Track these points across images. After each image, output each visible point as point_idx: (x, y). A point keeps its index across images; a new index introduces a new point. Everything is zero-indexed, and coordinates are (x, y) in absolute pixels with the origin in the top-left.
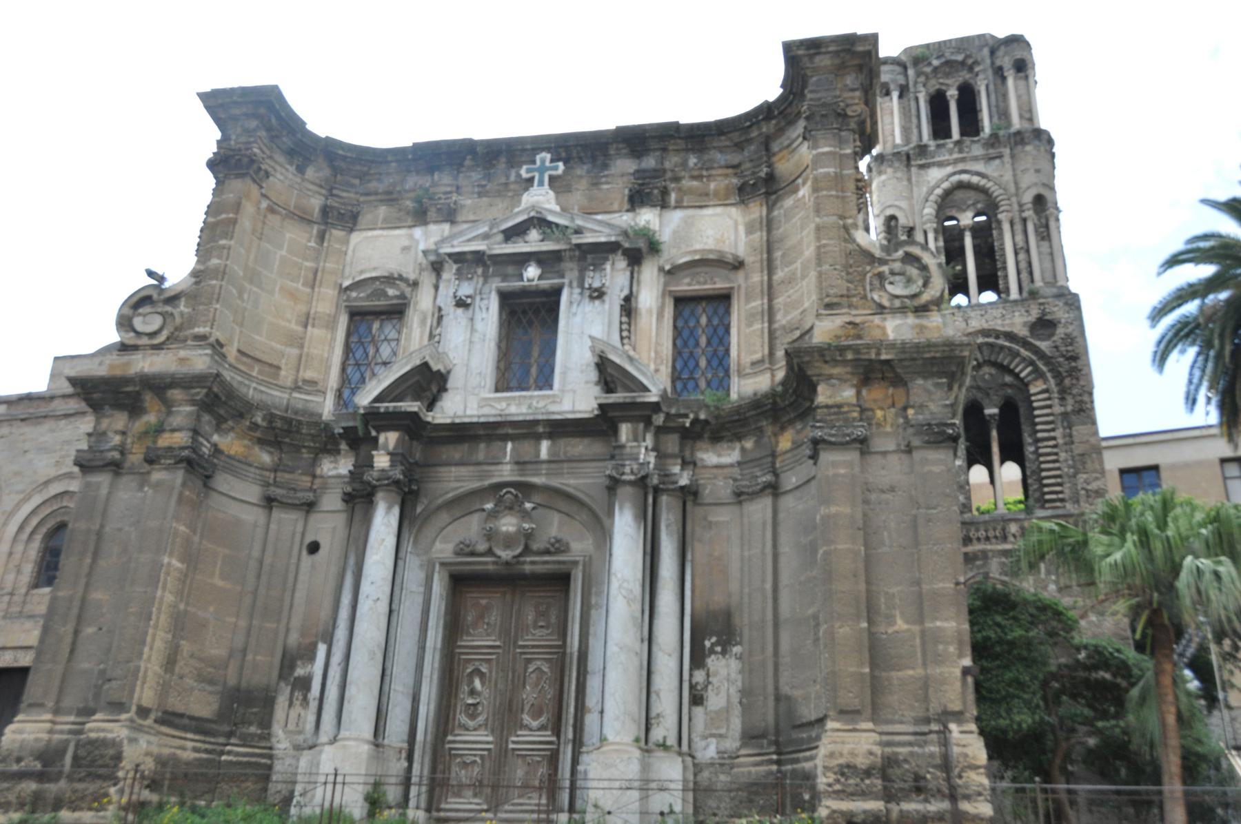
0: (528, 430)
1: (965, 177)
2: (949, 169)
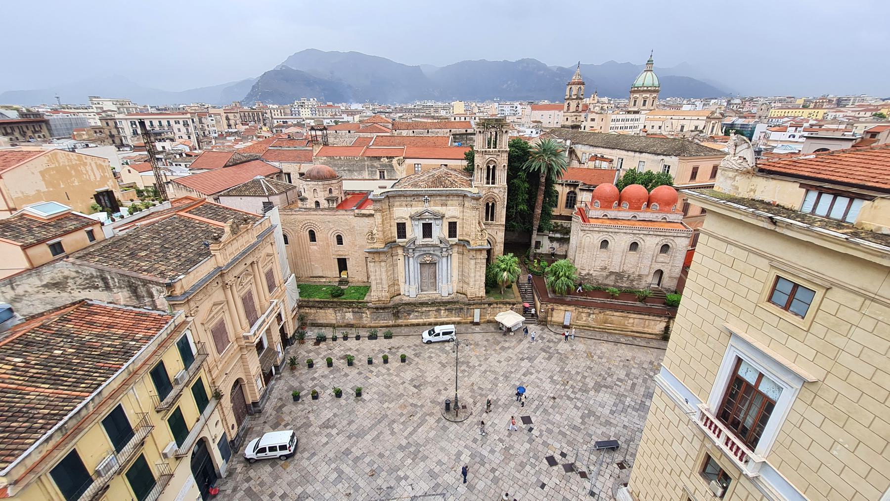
0: (427, 246)
1: (492, 159)
2: (490, 156)
